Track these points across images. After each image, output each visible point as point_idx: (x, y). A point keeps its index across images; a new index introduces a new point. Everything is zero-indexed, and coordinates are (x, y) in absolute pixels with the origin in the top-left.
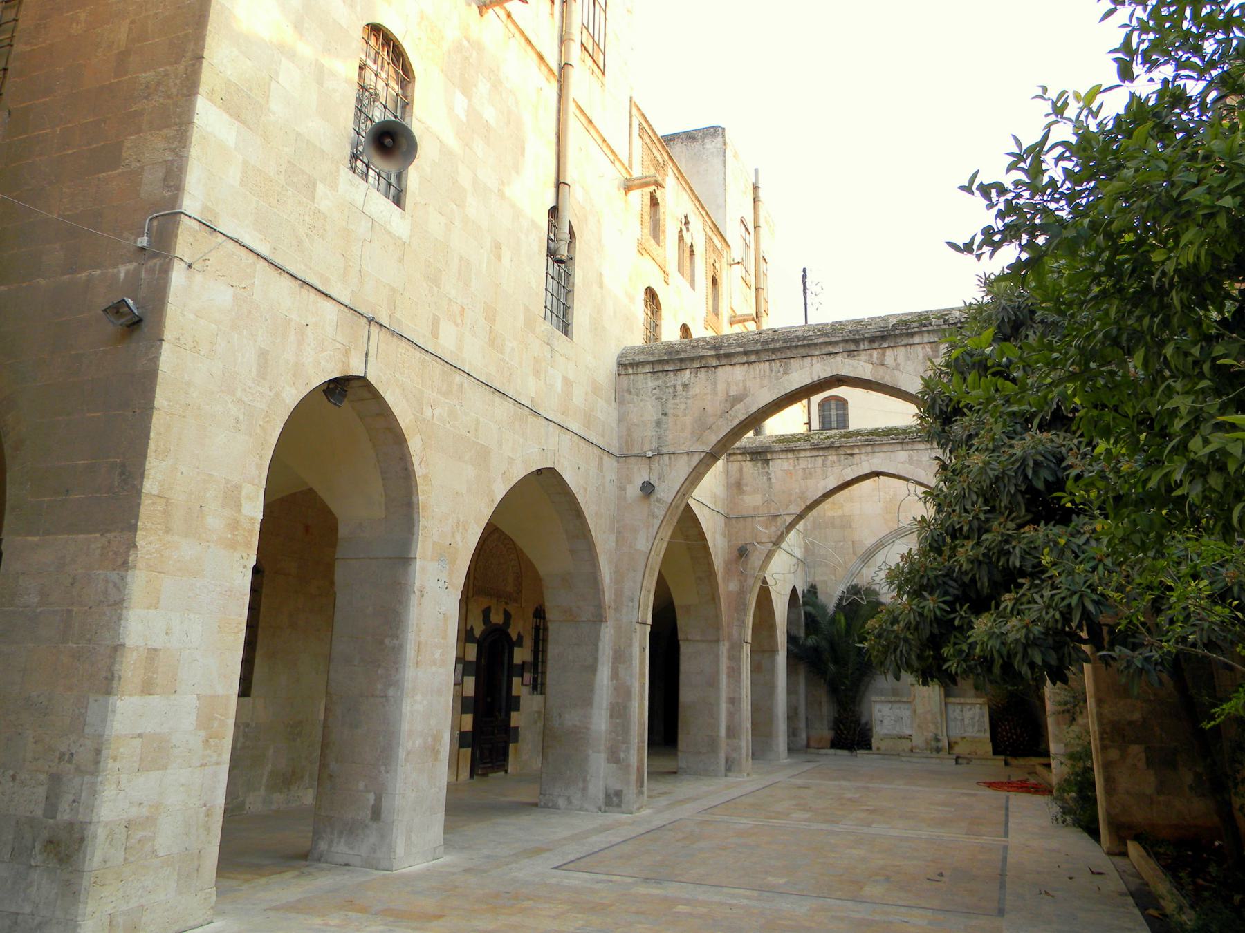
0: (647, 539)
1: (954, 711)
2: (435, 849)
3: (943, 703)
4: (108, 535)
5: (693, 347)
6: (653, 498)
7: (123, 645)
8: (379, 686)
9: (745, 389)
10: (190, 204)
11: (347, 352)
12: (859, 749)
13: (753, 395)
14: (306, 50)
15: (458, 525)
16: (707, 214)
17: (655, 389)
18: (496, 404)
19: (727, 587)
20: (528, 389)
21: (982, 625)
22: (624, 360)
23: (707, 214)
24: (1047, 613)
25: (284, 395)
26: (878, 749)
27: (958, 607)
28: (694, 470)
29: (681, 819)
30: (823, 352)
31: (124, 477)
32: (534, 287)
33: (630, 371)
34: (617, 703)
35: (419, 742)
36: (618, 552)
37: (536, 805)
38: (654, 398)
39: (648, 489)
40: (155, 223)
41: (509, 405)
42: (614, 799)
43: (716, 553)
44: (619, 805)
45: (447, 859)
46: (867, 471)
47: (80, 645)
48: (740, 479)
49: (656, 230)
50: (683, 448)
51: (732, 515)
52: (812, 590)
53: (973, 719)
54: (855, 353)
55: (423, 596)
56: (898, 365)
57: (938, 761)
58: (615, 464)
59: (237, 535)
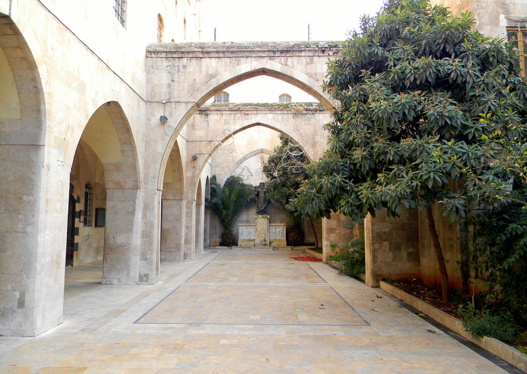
0: (163, 147)
2: (59, 319)
5: (189, 46)
6: (166, 125)
8: (20, 226)
9: (217, 71)
15: (68, 128)
17: (168, 67)
19: (187, 174)
22: (150, 49)
26: (240, 245)
33: (153, 56)
34: (146, 231)
35: (48, 259)
36: (146, 153)
37: (100, 283)
38: (167, 72)
39: (163, 120)
42: (144, 278)
43: (183, 158)
44: (147, 281)
45: (66, 323)
46: (254, 122)
51: (189, 140)
52: (214, 178)
54: (273, 58)
55: (49, 170)
56: (293, 66)
57: (266, 249)
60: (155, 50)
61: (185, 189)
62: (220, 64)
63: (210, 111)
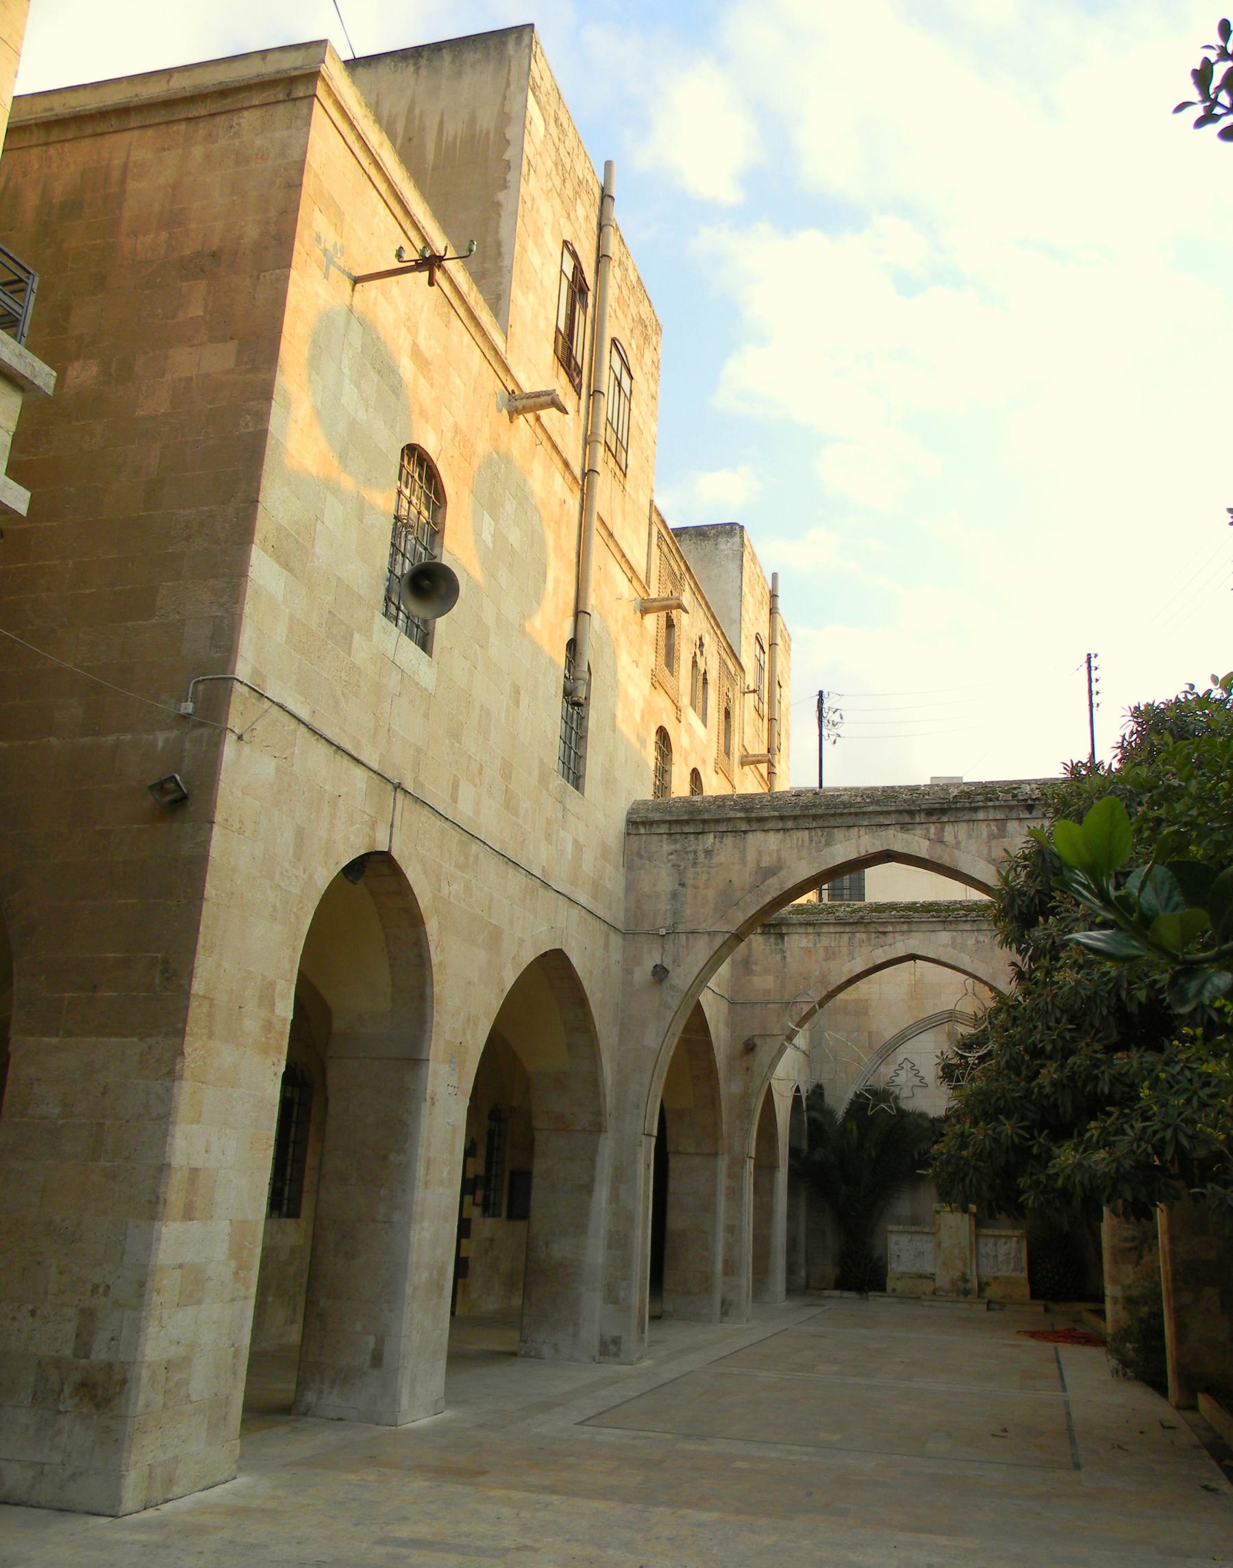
1: (986, 1245)
2: (437, 1401)
3: (974, 1236)
4: (148, 1039)
5: (719, 806)
7: (169, 1165)
9: (779, 859)
10: (242, 670)
11: (373, 825)
12: (870, 1291)
13: (788, 868)
14: (347, 483)
15: (469, 1020)
16: (722, 633)
17: (672, 854)
18: (510, 876)
19: (729, 1088)
20: (539, 856)
21: (1066, 1156)
23: (722, 633)
24: (1139, 1146)
25: (316, 878)
26: (894, 1290)
27: (1036, 1133)
28: (716, 953)
29: (691, 1372)
30: (873, 823)
31: (167, 975)
32: (549, 736)
33: (642, 831)
35: (425, 1275)
37: (514, 1354)
38: (669, 865)
40: (201, 687)
41: (521, 877)
44: (616, 1355)
45: (448, 1414)
46: (901, 953)
47: (116, 1164)
48: (749, 956)
49: (670, 656)
50: (703, 927)
52: (818, 1092)
53: (1007, 1254)
54: (910, 826)
55: (433, 1104)
56: (958, 843)
58: (620, 941)
59: (270, 1038)
60: (645, 819)
61: (725, 1127)
62: (788, 843)
63: (789, 925)
